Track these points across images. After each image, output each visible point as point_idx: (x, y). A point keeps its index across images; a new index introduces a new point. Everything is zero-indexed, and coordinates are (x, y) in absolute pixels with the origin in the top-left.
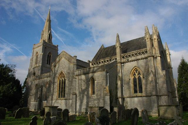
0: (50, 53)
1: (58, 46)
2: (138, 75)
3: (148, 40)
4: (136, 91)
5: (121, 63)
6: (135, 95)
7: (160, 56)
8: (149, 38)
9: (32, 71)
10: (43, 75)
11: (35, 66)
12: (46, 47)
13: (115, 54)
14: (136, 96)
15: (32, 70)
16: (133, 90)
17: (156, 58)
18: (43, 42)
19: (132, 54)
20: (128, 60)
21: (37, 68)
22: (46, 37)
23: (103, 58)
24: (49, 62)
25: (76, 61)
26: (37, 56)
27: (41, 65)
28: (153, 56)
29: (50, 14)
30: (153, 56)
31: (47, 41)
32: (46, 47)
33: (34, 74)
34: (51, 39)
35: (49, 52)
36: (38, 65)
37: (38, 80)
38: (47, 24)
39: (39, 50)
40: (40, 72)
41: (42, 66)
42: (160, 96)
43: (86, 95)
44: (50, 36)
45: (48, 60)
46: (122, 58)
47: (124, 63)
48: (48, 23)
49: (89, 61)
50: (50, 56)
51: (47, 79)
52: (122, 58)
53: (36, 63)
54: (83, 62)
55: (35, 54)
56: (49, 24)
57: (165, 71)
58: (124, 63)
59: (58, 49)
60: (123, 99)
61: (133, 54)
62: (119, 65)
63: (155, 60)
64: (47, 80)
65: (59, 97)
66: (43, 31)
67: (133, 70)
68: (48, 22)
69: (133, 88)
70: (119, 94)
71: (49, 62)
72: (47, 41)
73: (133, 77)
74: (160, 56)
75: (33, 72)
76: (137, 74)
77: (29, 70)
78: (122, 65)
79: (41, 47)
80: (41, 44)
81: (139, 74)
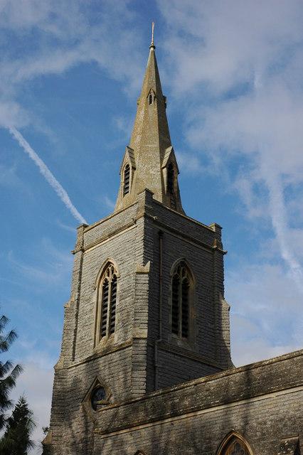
0: (183, 266)
1: (218, 227)
9: (76, 381)
10: (189, 390)
11: (101, 345)
12: (161, 233)
15: (77, 373)
21: (116, 356)
22: (150, 176)
24: (185, 324)
26: (109, 290)
27: (144, 333)
29: (156, 62)
31: (158, 197)
32: (161, 233)
33: (97, 393)
35: (177, 261)
36: (117, 338)
37: (145, 431)
38: (145, 114)
39: (127, 253)
40: (140, 376)
41: (154, 341)
43: (155, 439)
45: (175, 308)
48: (154, 108)
50: (186, 287)
51: (227, 413)
53: (106, 326)
55: (91, 276)
56: (159, 116)
59: (220, 245)
64: (227, 423)
66: (131, 151)
68: (154, 104)
71: (185, 324)
72: (158, 197)
75: (84, 385)
77: (59, 375)
79: (137, 234)
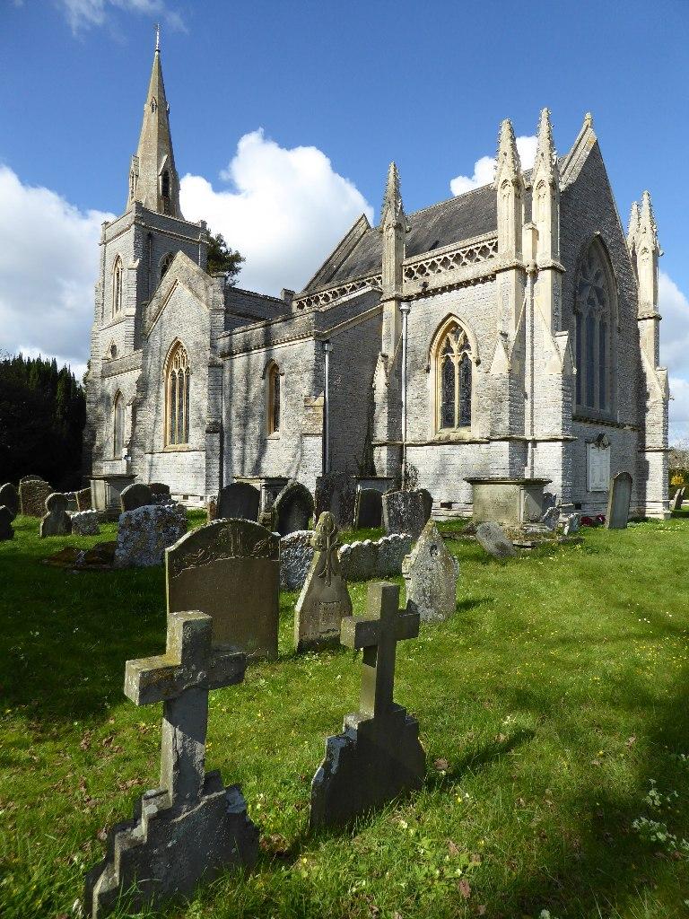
2: (462, 348)
3: (646, 255)
4: (448, 421)
5: (399, 300)
6: (446, 432)
7: (553, 268)
8: (650, 250)
12: (150, 236)
13: (374, 264)
14: (448, 437)
16: (440, 390)
17: (535, 274)
18: (134, 214)
19: (442, 257)
20: (425, 285)
22: (147, 189)
23: (93, 514)
25: (221, 297)
28: (518, 268)
30: (518, 268)
34: (176, 196)
42: (535, 442)
44: (166, 181)
46: (407, 275)
47: (409, 299)
49: (289, 293)
52: (404, 278)
54: (256, 296)
57: (566, 333)
58: (409, 299)
60: (398, 451)
61: (445, 258)
62: (390, 308)
63: (528, 289)
65: (172, 442)
67: (435, 344)
69: (439, 408)
70: (381, 433)
72: (153, 207)
73: (443, 361)
74: (553, 268)
76: (455, 346)
78: (404, 306)
79: (129, 236)
80: (130, 219)
81: (465, 346)
